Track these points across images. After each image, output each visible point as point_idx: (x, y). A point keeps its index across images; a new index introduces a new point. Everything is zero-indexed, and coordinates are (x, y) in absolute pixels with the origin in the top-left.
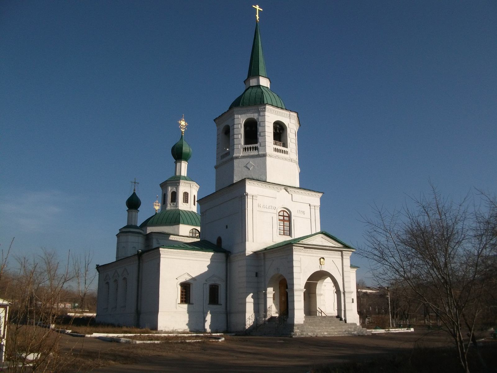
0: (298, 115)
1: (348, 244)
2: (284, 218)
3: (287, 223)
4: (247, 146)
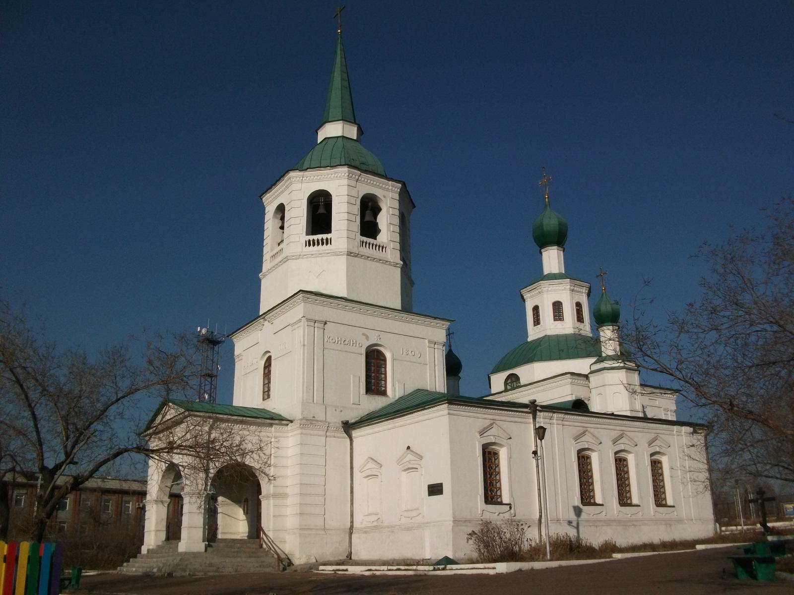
4: (311, 237)
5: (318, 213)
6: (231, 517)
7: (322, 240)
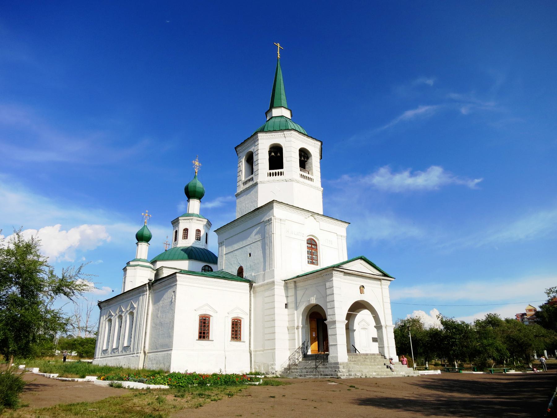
0: (322, 144)
1: (386, 272)
2: (312, 246)
3: (65, 385)
4: (272, 171)
5: (271, 155)
6: (270, 333)
7: (276, 173)
